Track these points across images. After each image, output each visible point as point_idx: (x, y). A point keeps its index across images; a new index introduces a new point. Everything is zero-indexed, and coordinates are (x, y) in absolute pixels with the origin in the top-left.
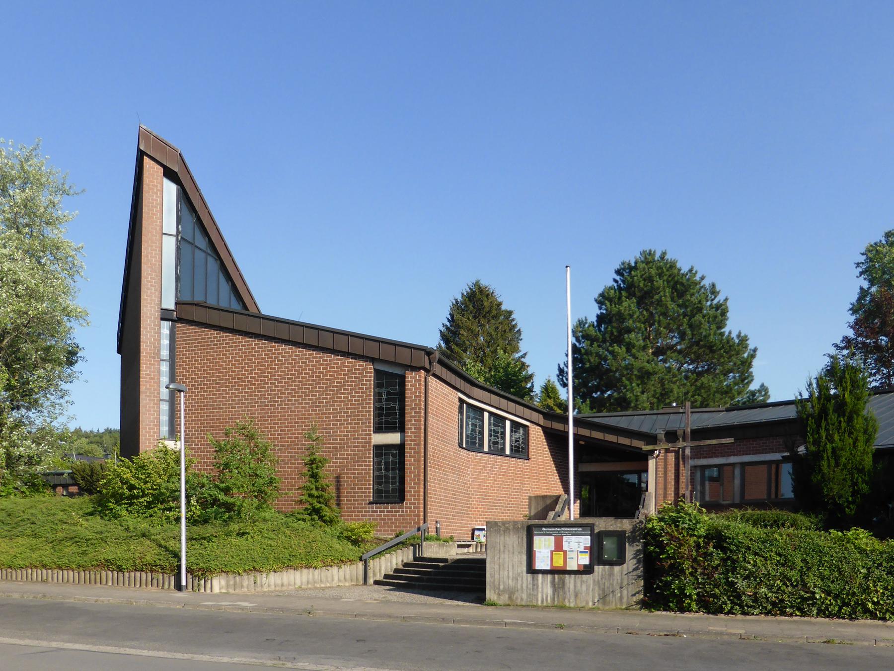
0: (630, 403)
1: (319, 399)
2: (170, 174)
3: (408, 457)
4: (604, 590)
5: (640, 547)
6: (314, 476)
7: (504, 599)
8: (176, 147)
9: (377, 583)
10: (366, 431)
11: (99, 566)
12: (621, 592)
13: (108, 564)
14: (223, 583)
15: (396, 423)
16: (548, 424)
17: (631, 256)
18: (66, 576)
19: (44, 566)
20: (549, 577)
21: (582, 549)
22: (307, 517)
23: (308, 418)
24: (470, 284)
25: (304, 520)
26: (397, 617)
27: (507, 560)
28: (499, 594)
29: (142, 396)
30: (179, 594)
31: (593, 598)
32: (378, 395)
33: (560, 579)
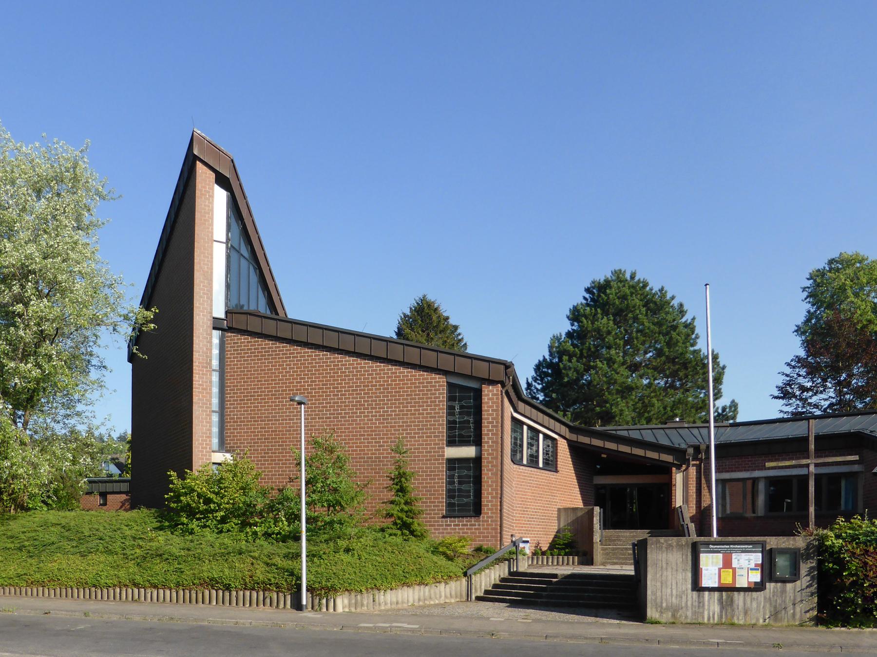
0: (614, 417)
1: (387, 411)
2: (222, 181)
3: (485, 471)
4: (775, 607)
5: (814, 564)
6: (402, 490)
7: (667, 617)
8: (229, 153)
9: (479, 599)
10: (439, 444)
11: (201, 584)
12: (794, 609)
13: (212, 583)
14: (346, 601)
15: (470, 436)
16: (573, 437)
17: (602, 274)
18: (161, 595)
19: (136, 585)
20: (716, 594)
21: (753, 566)
22: (399, 532)
23: (375, 431)
24: (417, 299)
25: (395, 535)
26: (594, 638)
27: (670, 577)
28: (661, 612)
29: (195, 407)
30: (301, 614)
31: (764, 614)
32: (450, 410)
33: (728, 597)
